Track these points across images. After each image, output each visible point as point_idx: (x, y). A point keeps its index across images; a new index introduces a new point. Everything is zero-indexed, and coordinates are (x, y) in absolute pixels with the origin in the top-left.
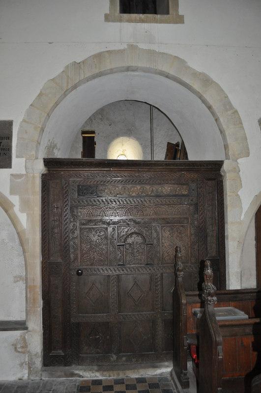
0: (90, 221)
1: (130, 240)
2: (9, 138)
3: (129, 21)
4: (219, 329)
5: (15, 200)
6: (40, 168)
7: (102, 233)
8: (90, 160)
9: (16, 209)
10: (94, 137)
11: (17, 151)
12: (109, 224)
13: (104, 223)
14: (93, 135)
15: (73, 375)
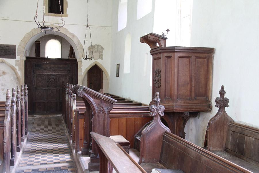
0: (39, 74)
1: (51, 80)
2: (15, 50)
3: (51, 16)
5: (17, 68)
6: (25, 59)
7: (42, 78)
9: (17, 70)
10: (61, 14)
11: (17, 54)
12: (44, 75)
13: (43, 75)
14: (61, 13)
15: (33, 116)
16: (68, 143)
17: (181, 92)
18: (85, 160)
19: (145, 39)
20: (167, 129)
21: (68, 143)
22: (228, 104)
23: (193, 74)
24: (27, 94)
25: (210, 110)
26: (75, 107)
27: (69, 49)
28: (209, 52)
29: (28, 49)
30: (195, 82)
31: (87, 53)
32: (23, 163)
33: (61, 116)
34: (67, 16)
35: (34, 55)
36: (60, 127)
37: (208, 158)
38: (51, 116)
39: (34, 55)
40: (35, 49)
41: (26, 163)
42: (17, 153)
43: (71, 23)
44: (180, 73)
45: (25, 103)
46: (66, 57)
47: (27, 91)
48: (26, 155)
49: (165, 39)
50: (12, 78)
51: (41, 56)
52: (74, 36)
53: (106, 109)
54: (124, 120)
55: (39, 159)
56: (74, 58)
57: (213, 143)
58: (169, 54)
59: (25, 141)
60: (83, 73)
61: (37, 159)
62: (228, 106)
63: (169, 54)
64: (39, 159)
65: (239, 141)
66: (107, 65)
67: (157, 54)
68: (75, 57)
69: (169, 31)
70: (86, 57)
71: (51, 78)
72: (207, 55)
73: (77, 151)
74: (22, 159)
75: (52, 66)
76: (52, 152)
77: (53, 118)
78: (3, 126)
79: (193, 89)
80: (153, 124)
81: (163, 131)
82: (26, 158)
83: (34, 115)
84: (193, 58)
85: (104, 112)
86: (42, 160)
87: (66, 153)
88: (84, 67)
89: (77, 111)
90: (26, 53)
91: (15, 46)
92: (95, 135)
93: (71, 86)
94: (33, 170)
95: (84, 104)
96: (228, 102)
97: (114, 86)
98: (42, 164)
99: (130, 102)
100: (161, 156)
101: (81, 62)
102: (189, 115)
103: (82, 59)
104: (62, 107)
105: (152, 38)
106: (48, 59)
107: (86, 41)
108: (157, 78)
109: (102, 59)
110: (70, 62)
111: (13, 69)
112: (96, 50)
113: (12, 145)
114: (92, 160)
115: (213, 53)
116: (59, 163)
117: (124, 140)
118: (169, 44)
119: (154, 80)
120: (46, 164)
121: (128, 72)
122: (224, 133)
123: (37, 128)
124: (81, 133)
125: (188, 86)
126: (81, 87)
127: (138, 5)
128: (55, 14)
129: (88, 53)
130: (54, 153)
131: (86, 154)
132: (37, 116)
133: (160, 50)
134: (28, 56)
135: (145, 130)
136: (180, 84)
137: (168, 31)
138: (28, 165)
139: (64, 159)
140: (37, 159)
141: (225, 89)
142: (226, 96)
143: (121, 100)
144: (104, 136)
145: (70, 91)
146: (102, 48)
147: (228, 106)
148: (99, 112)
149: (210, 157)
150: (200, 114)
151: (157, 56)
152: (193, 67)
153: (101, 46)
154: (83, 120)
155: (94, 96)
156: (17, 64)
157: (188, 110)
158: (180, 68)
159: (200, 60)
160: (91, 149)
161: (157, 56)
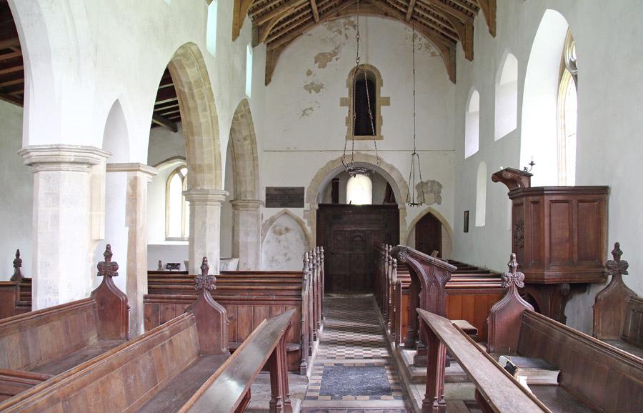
1: (356, 239)
2: (303, 195)
4: (186, 157)
5: (306, 221)
6: (317, 207)
8: (336, 204)
9: (306, 225)
15: (329, 296)
16: (384, 334)
17: (555, 254)
19: (498, 177)
20: (529, 307)
21: (383, 333)
22: (627, 270)
23: (575, 227)
24: (322, 260)
25: (604, 280)
27: (385, 188)
28: (604, 191)
29: (321, 192)
30: (578, 238)
32: (321, 356)
33: (372, 297)
34: (381, 138)
36: (370, 313)
37: (574, 338)
38: (356, 297)
39: (329, 201)
40: (332, 192)
41: (325, 356)
42: (314, 342)
43: (389, 148)
44: (555, 225)
45: (321, 272)
46: (380, 202)
47: (323, 257)
48: (324, 347)
49: (529, 176)
50: (298, 236)
51: (341, 202)
52: (392, 168)
53: (440, 279)
54: (470, 299)
55: (343, 352)
56: (393, 204)
57: (602, 328)
58: (536, 198)
59: (322, 328)
60: (408, 225)
61: (340, 352)
62: (626, 273)
63: (536, 198)
64: (343, 352)
66: (447, 213)
67: (518, 197)
68: (394, 201)
69: (532, 162)
70: (412, 202)
71: (357, 236)
72: (596, 197)
73: (397, 343)
74: (320, 350)
75: (358, 217)
76: (360, 345)
77: (360, 299)
78: (301, 301)
79: (576, 248)
80: (506, 299)
81: (523, 309)
82: (324, 350)
83: (331, 294)
84: (574, 202)
85: (437, 283)
86: (347, 354)
87: (380, 347)
88: (409, 217)
89: (398, 284)
90: (318, 198)
91: (303, 188)
93: (389, 248)
94: (335, 364)
95: (409, 275)
97: (459, 247)
98: (347, 358)
99: (485, 273)
100: (519, 344)
101: (404, 209)
102: (568, 287)
103: (407, 204)
104: (373, 281)
105: (509, 175)
106: (351, 206)
107: (412, 175)
108: (519, 234)
109: (439, 204)
110: (386, 209)
112: (429, 189)
113: (309, 327)
114: (420, 353)
115: (607, 194)
116: (371, 358)
117: (469, 326)
118: (535, 183)
119: (514, 237)
120: (353, 358)
121: (483, 224)
122: (620, 314)
123: (336, 312)
124: (403, 317)
125: (568, 245)
126: (404, 248)
127: (496, 118)
128: (363, 136)
129: (416, 195)
130: (364, 346)
131: (410, 346)
132: (335, 296)
133: (84, 385)
134: (321, 202)
135: (496, 307)
136: (553, 241)
137: (532, 164)
138: (328, 358)
139: (379, 354)
140: (340, 352)
141: (621, 248)
143: (464, 269)
145: (387, 255)
146: (440, 186)
147: (626, 273)
148: (430, 283)
149: (576, 337)
150: (590, 287)
151: (518, 201)
152: (575, 216)
153: (438, 183)
154: (406, 297)
155: (422, 261)
156: (305, 214)
157: (568, 280)
158: (553, 218)
160: (418, 340)
161: (518, 201)
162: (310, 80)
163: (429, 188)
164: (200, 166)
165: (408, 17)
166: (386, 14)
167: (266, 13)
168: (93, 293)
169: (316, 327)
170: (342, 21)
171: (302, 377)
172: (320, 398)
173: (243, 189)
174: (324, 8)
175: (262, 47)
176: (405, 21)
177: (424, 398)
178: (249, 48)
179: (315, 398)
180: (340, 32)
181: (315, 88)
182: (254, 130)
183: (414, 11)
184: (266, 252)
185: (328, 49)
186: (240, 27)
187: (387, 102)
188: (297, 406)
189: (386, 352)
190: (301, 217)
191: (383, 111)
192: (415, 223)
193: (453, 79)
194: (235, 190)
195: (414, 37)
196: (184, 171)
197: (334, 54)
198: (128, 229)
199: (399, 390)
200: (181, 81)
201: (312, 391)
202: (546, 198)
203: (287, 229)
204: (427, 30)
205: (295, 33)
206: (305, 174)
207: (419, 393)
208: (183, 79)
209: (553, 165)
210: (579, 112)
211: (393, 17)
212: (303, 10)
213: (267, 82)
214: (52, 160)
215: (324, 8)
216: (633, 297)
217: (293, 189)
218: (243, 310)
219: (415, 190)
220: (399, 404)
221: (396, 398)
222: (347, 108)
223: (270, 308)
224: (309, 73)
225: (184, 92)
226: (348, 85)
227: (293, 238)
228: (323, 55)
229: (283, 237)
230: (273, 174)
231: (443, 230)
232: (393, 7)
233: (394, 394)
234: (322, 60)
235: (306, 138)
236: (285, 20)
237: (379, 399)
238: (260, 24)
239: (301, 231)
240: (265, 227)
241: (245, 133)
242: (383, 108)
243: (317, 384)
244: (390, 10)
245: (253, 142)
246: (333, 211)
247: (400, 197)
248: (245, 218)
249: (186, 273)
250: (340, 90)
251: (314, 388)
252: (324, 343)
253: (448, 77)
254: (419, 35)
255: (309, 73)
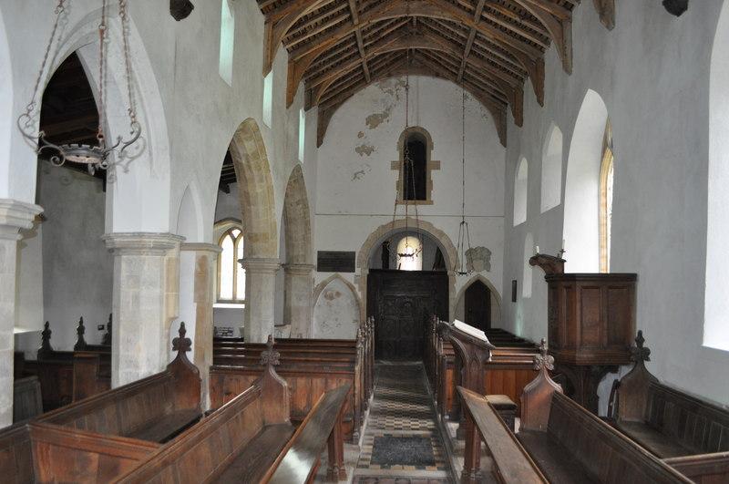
5: (356, 286)
9: (357, 290)
16: (431, 404)
18: (453, 427)
20: (558, 387)
21: (431, 404)
26: (442, 352)
31: (463, 260)
34: (431, 203)
35: (379, 266)
38: (406, 364)
39: (379, 266)
43: (438, 213)
44: (588, 314)
46: (430, 269)
51: (390, 268)
52: (442, 234)
53: (480, 357)
59: (372, 397)
62: (648, 359)
65: (680, 417)
66: (495, 279)
73: (443, 416)
81: (552, 391)
88: (459, 284)
91: (354, 253)
92: (465, 392)
96: (649, 354)
104: (423, 350)
110: (436, 275)
111: (352, 288)
112: (479, 256)
116: (418, 429)
131: (454, 420)
135: (527, 388)
142: (645, 345)
144: (222, 172)
156: (355, 279)
159: (615, 291)
162: (361, 142)
163: (478, 256)
164: (256, 235)
165: (460, 78)
166: (437, 75)
167: (318, 76)
168: (169, 366)
169: (367, 397)
170: (393, 80)
171: (354, 446)
172: (371, 466)
173: (295, 254)
174: (376, 69)
175: (315, 110)
176: (456, 82)
177: (462, 469)
178: (301, 112)
179: (367, 467)
180: (391, 92)
181: (365, 150)
182: (306, 195)
183: (474, 45)
184: (317, 317)
185: (380, 111)
186: (294, 95)
187: (437, 165)
188: (351, 472)
189: (432, 423)
190: (353, 282)
191: (435, 176)
192: (464, 289)
193: (504, 142)
194: (288, 254)
195: (465, 97)
196: (236, 233)
197: (385, 115)
198: (195, 304)
199: (443, 462)
200: (239, 153)
201: (362, 460)
202: (578, 284)
203: (338, 294)
204: (478, 93)
205: (347, 94)
206: (355, 239)
207: (459, 465)
208: (241, 151)
209: (586, 254)
210: (709, 73)
211: (444, 77)
212: (355, 71)
213: (319, 143)
214: (137, 244)
215: (376, 69)
216: (655, 381)
217: (344, 253)
218: (301, 382)
219: (465, 257)
220: (441, 474)
221: (439, 469)
222: (397, 172)
223: (326, 380)
224: (360, 135)
225: (241, 164)
226: (399, 148)
227: (345, 301)
228: (375, 116)
229: (334, 302)
230: (325, 238)
231: (492, 297)
232: (444, 67)
233: (437, 465)
234: (374, 121)
235: (354, 199)
236: (339, 81)
237: (424, 468)
238: (313, 87)
239: (352, 295)
240: (317, 291)
241: (298, 197)
242: (433, 172)
243: (368, 454)
244: (441, 71)
245: (306, 206)
246: (383, 276)
247: (450, 261)
248: (296, 281)
249: (242, 340)
250: (391, 151)
251: (366, 457)
252: (374, 413)
253: (498, 139)
254: (470, 96)
255: (360, 135)
